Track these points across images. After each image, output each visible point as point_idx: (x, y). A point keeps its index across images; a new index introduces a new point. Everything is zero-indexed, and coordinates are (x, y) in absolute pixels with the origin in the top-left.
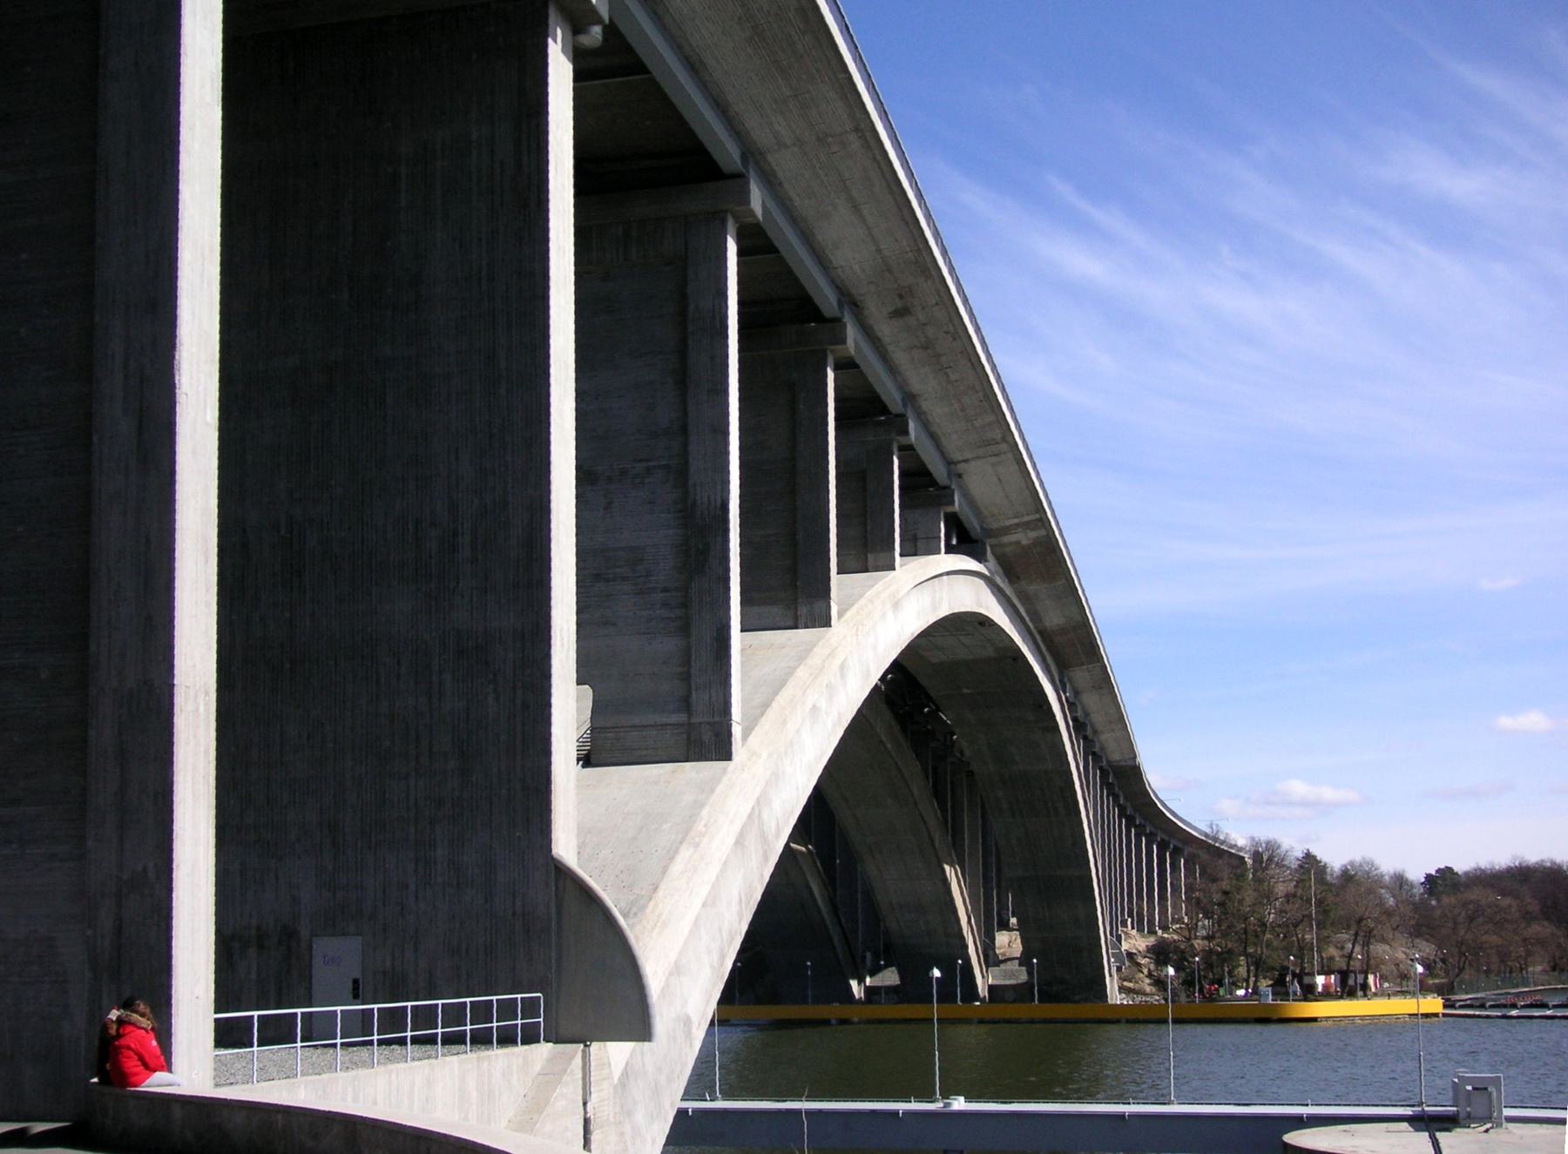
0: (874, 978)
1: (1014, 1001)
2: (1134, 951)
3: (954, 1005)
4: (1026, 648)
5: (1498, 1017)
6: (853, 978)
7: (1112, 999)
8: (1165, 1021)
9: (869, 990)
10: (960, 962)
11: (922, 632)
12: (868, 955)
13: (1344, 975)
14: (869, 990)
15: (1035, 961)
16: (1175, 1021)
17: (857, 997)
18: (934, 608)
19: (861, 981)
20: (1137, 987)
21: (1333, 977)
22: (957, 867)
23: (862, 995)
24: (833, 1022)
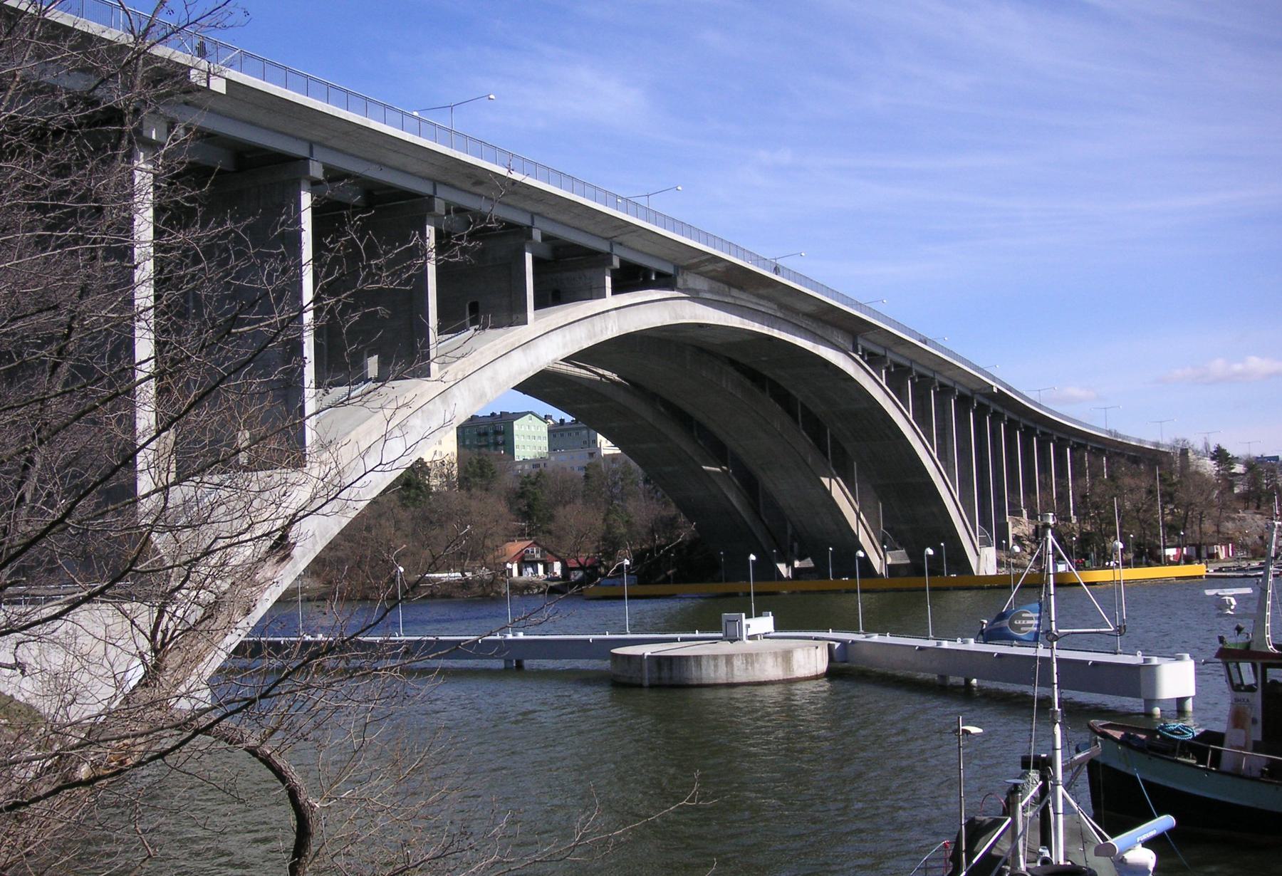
0: (803, 562)
1: (906, 576)
2: (1021, 535)
3: (826, 581)
4: (757, 325)
5: (1241, 577)
6: (781, 562)
7: (978, 572)
8: (622, 598)
9: (795, 571)
10: (831, 549)
11: (628, 333)
12: (796, 545)
13: (1198, 548)
14: (795, 571)
15: (942, 544)
16: (630, 598)
17: (785, 576)
18: (565, 345)
19: (789, 564)
20: (1019, 562)
21: (1185, 549)
22: (838, 479)
23: (790, 575)
24: (741, 594)
